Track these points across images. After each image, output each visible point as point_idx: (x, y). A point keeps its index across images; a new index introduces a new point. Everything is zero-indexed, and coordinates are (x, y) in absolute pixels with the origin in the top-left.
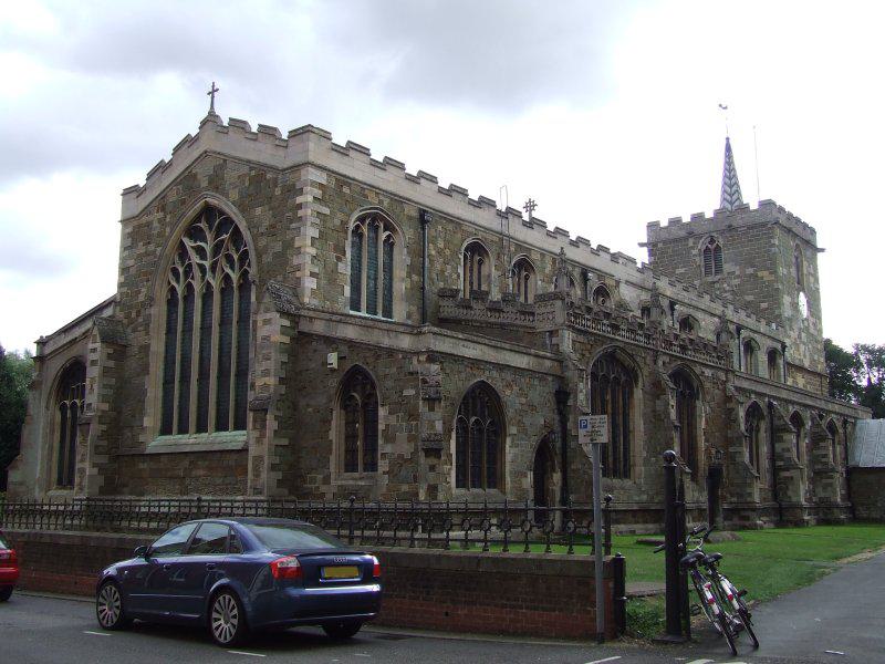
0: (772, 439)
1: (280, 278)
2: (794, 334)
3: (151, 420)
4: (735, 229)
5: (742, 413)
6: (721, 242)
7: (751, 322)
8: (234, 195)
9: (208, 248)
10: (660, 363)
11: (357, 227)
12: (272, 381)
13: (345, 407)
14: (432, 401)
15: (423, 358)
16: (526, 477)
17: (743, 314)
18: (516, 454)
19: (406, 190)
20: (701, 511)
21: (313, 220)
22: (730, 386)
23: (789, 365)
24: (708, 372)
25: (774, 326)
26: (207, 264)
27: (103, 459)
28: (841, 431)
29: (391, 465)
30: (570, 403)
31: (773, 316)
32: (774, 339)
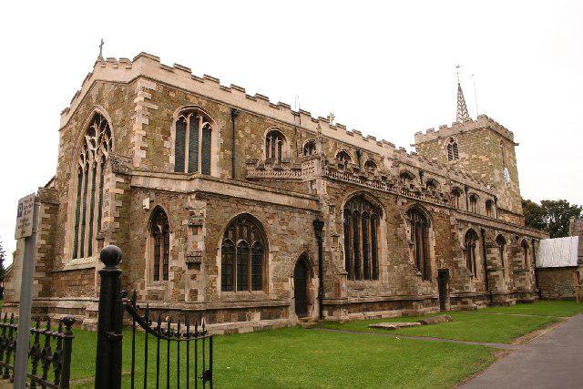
2: (502, 192)
5: (461, 235)
6: (457, 141)
9: (96, 139)
10: (399, 203)
11: (182, 119)
13: (154, 235)
14: (195, 227)
15: (193, 197)
18: (279, 268)
19: (218, 95)
20: (433, 300)
22: (452, 219)
24: (436, 210)
26: (95, 149)
27: (42, 275)
29: (176, 276)
30: (324, 229)
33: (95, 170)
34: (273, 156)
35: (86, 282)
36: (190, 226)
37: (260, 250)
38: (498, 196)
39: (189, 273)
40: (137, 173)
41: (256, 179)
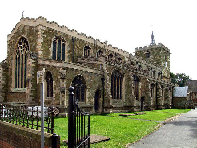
0: (157, 90)
1: (35, 52)
2: (164, 70)
3: (13, 85)
4: (153, 49)
5: (150, 85)
7: (155, 67)
8: (26, 34)
9: (22, 46)
10: (130, 73)
11: (55, 40)
12: (30, 75)
15: (62, 68)
16: (92, 99)
17: (153, 66)
18: (89, 94)
20: (139, 107)
21: (41, 38)
22: (147, 79)
23: (162, 76)
24: (142, 76)
25: (160, 68)
26: (22, 50)
27: (4, 94)
28: (172, 89)
31: (160, 66)
32: (159, 71)
33: (22, 57)
34: (87, 55)
35: (21, 97)
36: (61, 79)
37: (84, 88)
38: (162, 71)
39: (61, 95)
40: (40, 59)
41: (81, 63)
